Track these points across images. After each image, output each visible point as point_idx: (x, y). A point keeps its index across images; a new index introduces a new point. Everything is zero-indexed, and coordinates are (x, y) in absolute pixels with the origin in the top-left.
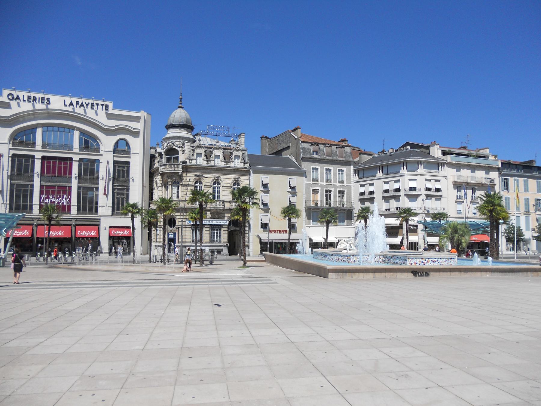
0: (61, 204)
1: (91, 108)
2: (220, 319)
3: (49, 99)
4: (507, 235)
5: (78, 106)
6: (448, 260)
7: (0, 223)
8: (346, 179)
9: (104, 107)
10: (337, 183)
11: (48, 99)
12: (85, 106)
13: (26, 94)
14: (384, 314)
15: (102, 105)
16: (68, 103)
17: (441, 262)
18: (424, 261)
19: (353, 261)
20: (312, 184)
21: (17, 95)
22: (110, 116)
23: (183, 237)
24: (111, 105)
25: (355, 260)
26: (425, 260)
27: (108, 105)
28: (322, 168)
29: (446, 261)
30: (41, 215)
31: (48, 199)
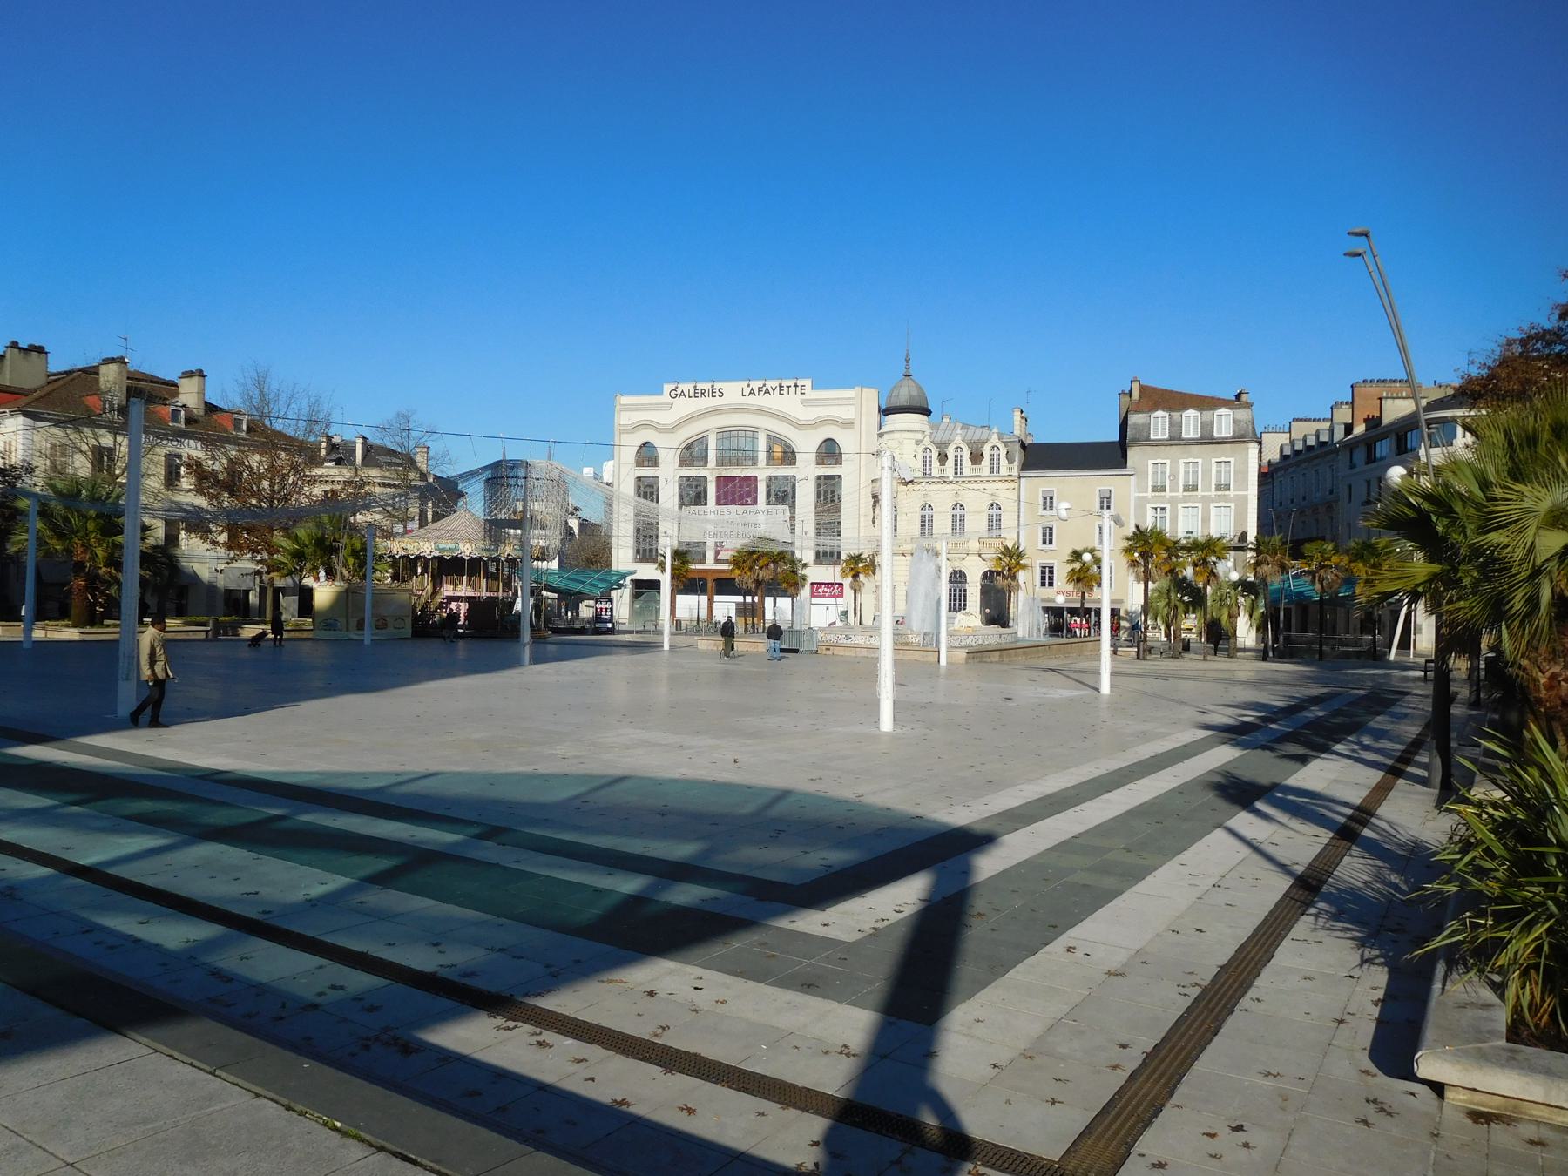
1: (780, 394)
2: (983, 764)
4: (1448, 568)
5: (761, 393)
7: (9, 892)
9: (799, 389)
10: (1147, 492)
12: (771, 392)
13: (691, 386)
15: (796, 386)
16: (747, 391)
21: (1211, 797)
22: (806, 403)
24: (807, 383)
28: (1175, 462)
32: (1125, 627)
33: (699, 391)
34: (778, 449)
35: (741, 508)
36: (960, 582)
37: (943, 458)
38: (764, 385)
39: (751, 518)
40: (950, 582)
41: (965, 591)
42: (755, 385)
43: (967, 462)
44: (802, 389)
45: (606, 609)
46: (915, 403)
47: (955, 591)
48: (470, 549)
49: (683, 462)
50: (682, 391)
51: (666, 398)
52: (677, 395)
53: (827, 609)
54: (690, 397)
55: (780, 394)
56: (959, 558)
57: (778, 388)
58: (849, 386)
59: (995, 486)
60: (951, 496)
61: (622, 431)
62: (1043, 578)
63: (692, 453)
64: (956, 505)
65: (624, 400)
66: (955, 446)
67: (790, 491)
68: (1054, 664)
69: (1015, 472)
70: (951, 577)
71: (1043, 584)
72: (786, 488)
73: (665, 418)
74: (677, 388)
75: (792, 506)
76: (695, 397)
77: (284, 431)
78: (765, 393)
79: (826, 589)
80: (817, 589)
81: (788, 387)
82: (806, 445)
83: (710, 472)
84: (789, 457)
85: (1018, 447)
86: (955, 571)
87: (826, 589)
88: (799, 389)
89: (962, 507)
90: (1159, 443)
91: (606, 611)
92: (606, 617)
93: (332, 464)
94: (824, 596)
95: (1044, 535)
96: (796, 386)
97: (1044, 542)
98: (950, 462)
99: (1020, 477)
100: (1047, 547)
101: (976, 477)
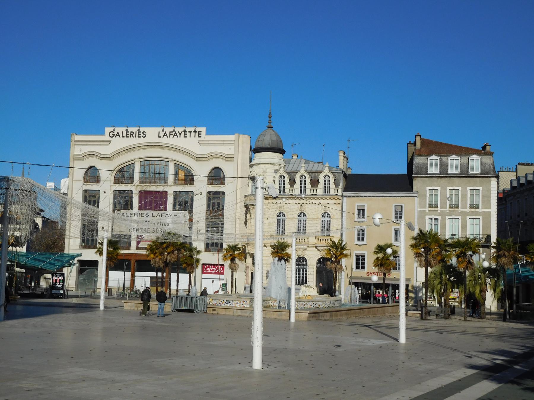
0: (217, 272)
1: (184, 137)
3: (145, 132)
5: (172, 136)
6: (240, 303)
8: (482, 202)
9: (197, 134)
11: (144, 133)
12: (178, 135)
13: (124, 130)
15: (195, 132)
16: (162, 134)
17: (233, 304)
18: (220, 302)
19: (209, 302)
20: (469, 212)
23: (120, 290)
24: (203, 130)
25: (210, 302)
26: (221, 302)
27: (201, 132)
29: (238, 303)
31: (208, 268)
32: (411, 297)
33: (130, 133)
34: (182, 174)
35: (155, 213)
36: (303, 265)
37: (292, 182)
38: (174, 131)
41: (306, 271)
42: (168, 130)
43: (308, 186)
44: (199, 134)
45: (60, 280)
47: (299, 271)
49: (117, 181)
50: (118, 133)
51: (106, 137)
52: (114, 135)
53: (213, 282)
54: (123, 137)
55: (184, 137)
56: (302, 249)
59: (326, 201)
65: (78, 137)
66: (300, 174)
67: (189, 200)
69: (340, 193)
71: (358, 267)
74: (114, 130)
75: (191, 212)
76: (126, 137)
78: (174, 135)
79: (212, 269)
80: (206, 268)
81: (190, 132)
83: (135, 188)
87: (212, 269)
91: (60, 282)
94: (211, 273)
95: (359, 235)
96: (195, 132)
98: (297, 186)
99: (343, 196)
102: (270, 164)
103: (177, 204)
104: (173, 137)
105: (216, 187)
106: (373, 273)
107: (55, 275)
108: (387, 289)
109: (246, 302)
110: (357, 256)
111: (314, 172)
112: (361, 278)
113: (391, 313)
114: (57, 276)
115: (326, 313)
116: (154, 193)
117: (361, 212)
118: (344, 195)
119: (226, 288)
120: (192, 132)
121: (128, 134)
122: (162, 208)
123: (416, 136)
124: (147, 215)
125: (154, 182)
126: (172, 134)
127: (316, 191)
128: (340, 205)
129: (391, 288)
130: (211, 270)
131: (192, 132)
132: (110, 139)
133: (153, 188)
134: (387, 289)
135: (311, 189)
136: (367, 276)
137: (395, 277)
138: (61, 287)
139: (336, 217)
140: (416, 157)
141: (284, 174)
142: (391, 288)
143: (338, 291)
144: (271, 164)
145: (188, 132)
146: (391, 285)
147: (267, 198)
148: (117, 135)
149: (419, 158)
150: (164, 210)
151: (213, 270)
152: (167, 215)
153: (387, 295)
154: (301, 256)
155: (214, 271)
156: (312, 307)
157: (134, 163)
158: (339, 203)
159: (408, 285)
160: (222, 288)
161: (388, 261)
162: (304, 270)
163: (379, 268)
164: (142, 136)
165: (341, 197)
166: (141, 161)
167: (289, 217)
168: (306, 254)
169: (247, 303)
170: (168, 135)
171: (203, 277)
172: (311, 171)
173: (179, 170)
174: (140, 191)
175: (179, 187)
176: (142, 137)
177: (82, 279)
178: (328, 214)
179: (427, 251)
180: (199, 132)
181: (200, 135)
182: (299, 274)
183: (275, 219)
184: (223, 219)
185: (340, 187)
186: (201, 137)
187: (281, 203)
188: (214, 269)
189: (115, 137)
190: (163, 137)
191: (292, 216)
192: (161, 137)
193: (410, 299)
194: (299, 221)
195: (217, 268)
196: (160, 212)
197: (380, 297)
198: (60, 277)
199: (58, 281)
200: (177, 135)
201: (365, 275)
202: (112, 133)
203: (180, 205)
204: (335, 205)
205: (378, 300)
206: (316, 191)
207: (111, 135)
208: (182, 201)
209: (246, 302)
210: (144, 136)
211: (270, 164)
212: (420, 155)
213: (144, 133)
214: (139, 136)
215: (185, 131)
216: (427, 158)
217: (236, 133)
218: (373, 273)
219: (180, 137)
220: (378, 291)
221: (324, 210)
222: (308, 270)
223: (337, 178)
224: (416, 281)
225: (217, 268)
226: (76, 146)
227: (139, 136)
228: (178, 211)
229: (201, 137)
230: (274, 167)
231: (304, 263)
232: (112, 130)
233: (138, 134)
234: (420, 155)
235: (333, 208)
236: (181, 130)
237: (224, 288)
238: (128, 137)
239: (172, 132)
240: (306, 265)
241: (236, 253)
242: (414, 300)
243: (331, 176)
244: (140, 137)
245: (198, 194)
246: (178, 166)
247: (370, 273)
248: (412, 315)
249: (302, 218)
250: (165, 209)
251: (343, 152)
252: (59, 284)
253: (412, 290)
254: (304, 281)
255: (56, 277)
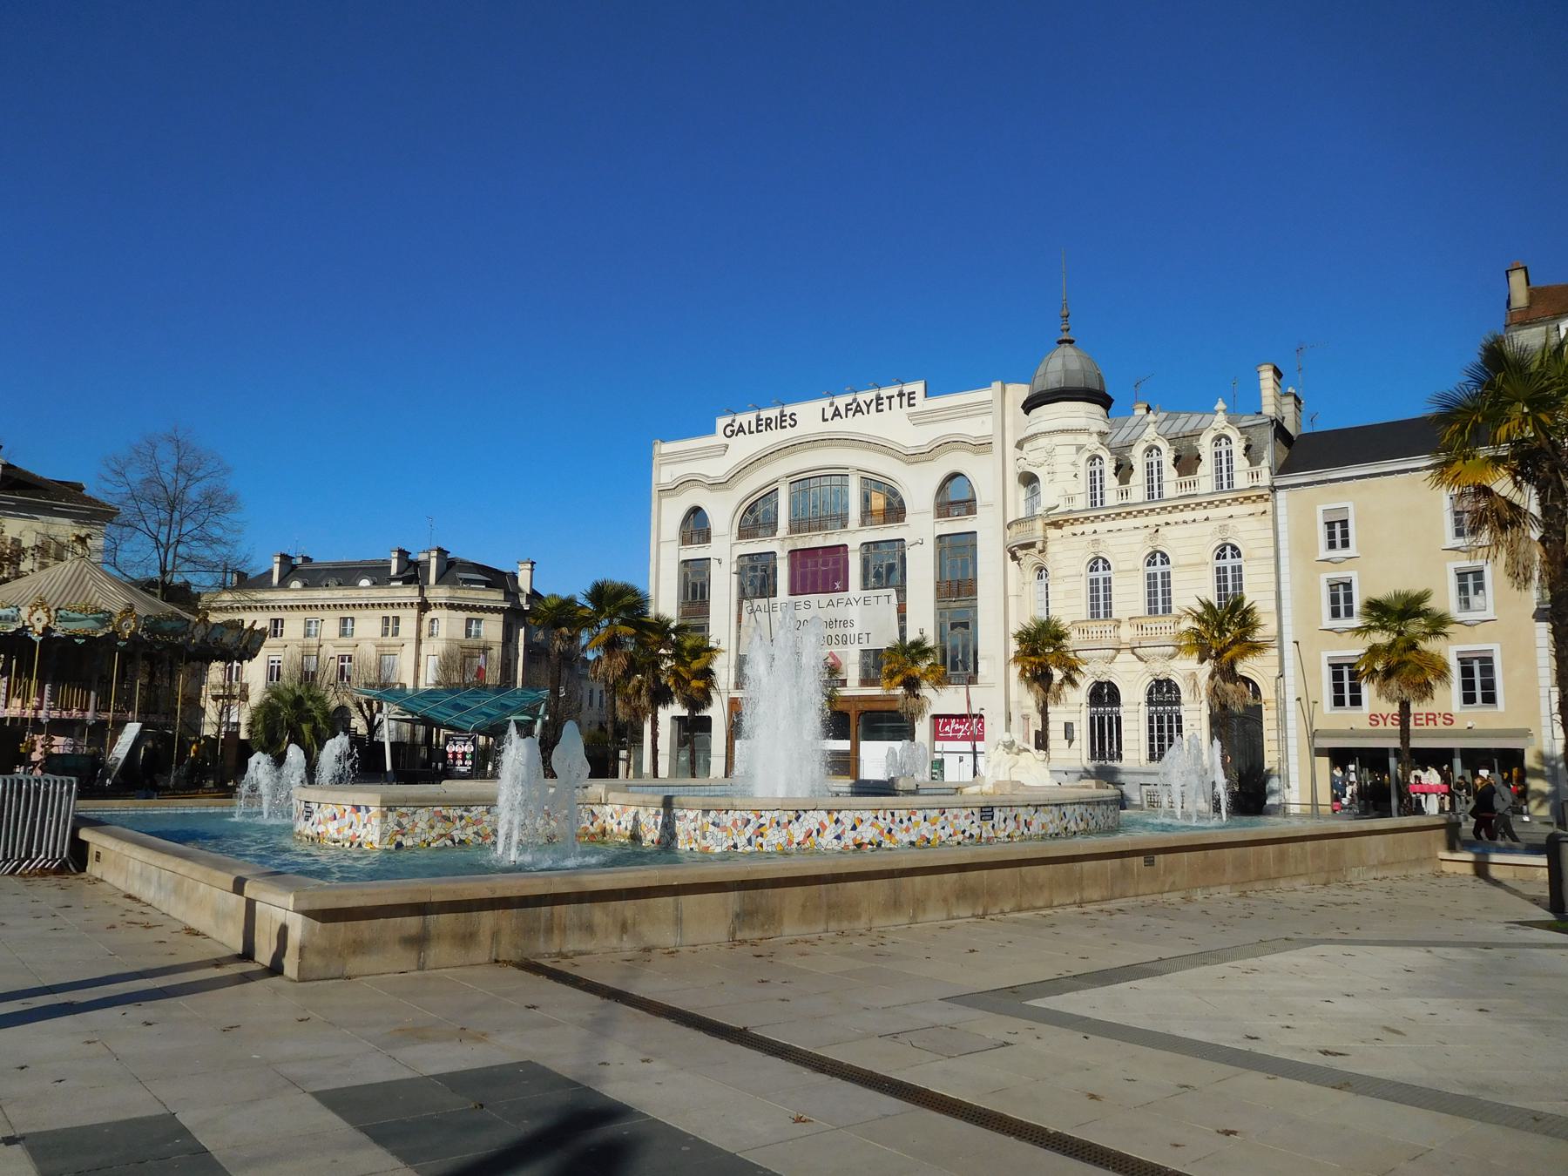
0: (968, 734)
1: (878, 411)
3: (795, 414)
5: (850, 413)
9: (905, 399)
11: (793, 417)
12: (864, 408)
13: (752, 416)
14: (1288, 1027)
16: (829, 412)
22: (918, 420)
24: (918, 387)
27: (914, 393)
30: (26, 863)
31: (948, 727)
32: (1540, 794)
33: (764, 422)
34: (878, 502)
35: (824, 598)
36: (1170, 703)
37: (1123, 470)
38: (855, 400)
39: (837, 613)
40: (1150, 702)
41: (1179, 719)
42: (841, 401)
43: (1170, 473)
44: (909, 399)
45: (464, 754)
46: (1077, 382)
47: (1160, 720)
48: (45, 620)
49: (745, 533)
50: (741, 425)
51: (718, 438)
52: (733, 431)
53: (961, 760)
55: (878, 411)
56: (1163, 656)
57: (874, 402)
58: (983, 383)
59: (1225, 511)
60: (1142, 537)
61: (662, 494)
62: (1338, 688)
63: (755, 520)
64: (1153, 555)
65: (666, 448)
66: (1145, 445)
67: (897, 561)
68: (1289, 672)
69: (1265, 479)
70: (1150, 693)
71: (1339, 702)
72: (891, 561)
73: (717, 468)
74: (734, 421)
75: (901, 591)
76: (758, 431)
77: (1298, 789)
78: (856, 411)
79: (957, 727)
80: (944, 725)
81: (890, 398)
82: (919, 490)
83: (779, 545)
84: (895, 511)
85: (1269, 433)
86: (1159, 683)
87: (957, 727)
88: (905, 399)
89: (1165, 559)
90: (1470, 573)
91: (464, 759)
92: (463, 769)
93: (400, 583)
94: (954, 739)
95: (1334, 599)
96: (901, 395)
97: (1332, 545)
98: (1138, 478)
99: (1274, 489)
100: (1339, 553)
101: (1189, 503)
102: (1062, 431)
103: (872, 572)
104: (854, 416)
105: (956, 522)
106: (1390, 717)
107: (453, 740)
108: (1445, 767)
109: (368, 810)
110: (1333, 666)
111: (1186, 434)
112: (1352, 733)
113: (1384, 864)
114: (457, 742)
115: (769, 892)
116: (820, 552)
117: (1338, 531)
118: (1276, 484)
119: (942, 772)
120: (893, 397)
121: (762, 425)
122: (838, 587)
123: (1507, 272)
124: (808, 605)
125: (819, 525)
126: (851, 409)
127: (1192, 484)
128: (1269, 517)
129: (1457, 762)
130: (954, 731)
131: (893, 397)
132: (727, 441)
133: (817, 540)
134: (1445, 767)
135: (1178, 482)
136: (1372, 728)
137: (1470, 726)
138: (468, 770)
139: (1259, 553)
140: (1516, 331)
141: (1100, 452)
142: (1457, 762)
143: (1279, 777)
144: (1068, 430)
145: (885, 398)
146: (1457, 753)
147: (1058, 521)
148: (739, 431)
149: (1525, 331)
150: (844, 591)
151: (959, 730)
152: (849, 602)
153: (1446, 786)
154: (1161, 677)
155: (961, 734)
156: (827, 840)
157: (777, 489)
158: (1264, 512)
159: (1523, 750)
160: (932, 773)
161: (1411, 656)
162: (1172, 716)
163: (1379, 685)
164: (790, 424)
165: (1268, 492)
166: (791, 483)
167: (1122, 566)
168: (1176, 669)
169: (369, 820)
170: (843, 413)
171: (936, 750)
172: (1177, 433)
173: (873, 493)
174: (790, 552)
175: (872, 532)
176: (788, 426)
177: (683, 759)
178: (1234, 548)
179: (1553, 470)
180: (910, 394)
181: (912, 402)
182: (1160, 729)
183: (1083, 578)
184: (976, 599)
185: (1265, 463)
186: (914, 405)
187: (1095, 532)
188: (962, 727)
189: (737, 435)
190: (832, 419)
191: (1129, 566)
192: (827, 420)
193: (1533, 798)
194: (1151, 577)
195: (967, 724)
196: (835, 596)
197: (1422, 793)
198: (465, 745)
199: (459, 756)
200: (861, 411)
201: (1364, 725)
202: (730, 428)
203: (878, 575)
204: (1251, 518)
205: (1414, 802)
206: (1192, 484)
207: (729, 433)
208: (881, 566)
209: (368, 810)
210: (793, 423)
211: (1062, 431)
212: (1527, 324)
213: (793, 417)
214: (784, 424)
215: (879, 398)
216: (1556, 325)
217: (995, 381)
218: (1390, 717)
219: (868, 413)
220: (1414, 773)
221: (1221, 537)
222: (1183, 713)
223: (1254, 441)
224: (1550, 738)
225: (967, 724)
226: (663, 468)
227: (784, 424)
228: (874, 589)
229: (914, 405)
230: (1076, 439)
231: (1171, 697)
232: (728, 420)
233: (782, 421)
234: (1530, 323)
235: (1248, 529)
236: (869, 395)
237: (936, 773)
238: (762, 431)
239: (851, 404)
240: (1178, 702)
241: (924, 665)
242: (1551, 801)
243: (1234, 434)
244: (785, 427)
245: (916, 544)
246: (872, 483)
247: (1381, 715)
248: (1512, 875)
249: (1159, 569)
250: (846, 589)
251: (1272, 367)
252: (464, 765)
253: (1538, 767)
254: (1156, 750)
255: (455, 745)
